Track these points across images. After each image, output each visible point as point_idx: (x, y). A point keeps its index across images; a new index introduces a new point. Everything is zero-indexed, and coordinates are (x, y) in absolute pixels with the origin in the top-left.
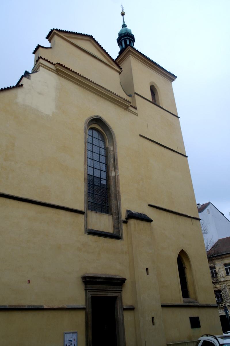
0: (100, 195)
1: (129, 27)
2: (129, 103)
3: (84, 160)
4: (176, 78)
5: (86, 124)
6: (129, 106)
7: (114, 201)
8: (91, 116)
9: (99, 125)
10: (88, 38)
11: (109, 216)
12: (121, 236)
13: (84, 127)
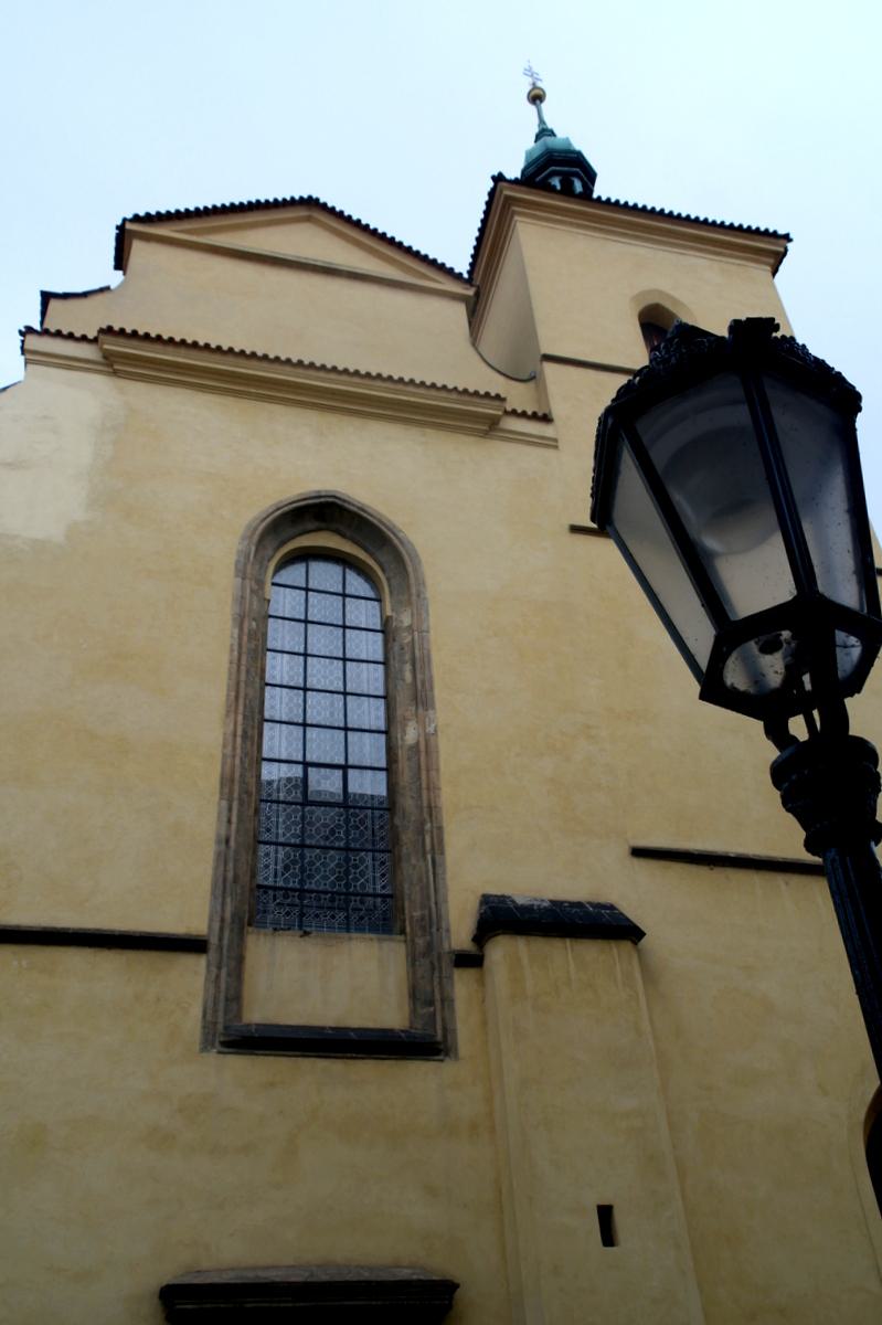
0: (338, 849)
1: (561, 134)
2: (497, 403)
3: (228, 695)
4: (790, 240)
5: (251, 537)
6: (500, 413)
7: (413, 861)
8: (281, 501)
9: (343, 536)
10: (302, 212)
11: (386, 945)
12: (445, 1036)
13: (239, 552)
